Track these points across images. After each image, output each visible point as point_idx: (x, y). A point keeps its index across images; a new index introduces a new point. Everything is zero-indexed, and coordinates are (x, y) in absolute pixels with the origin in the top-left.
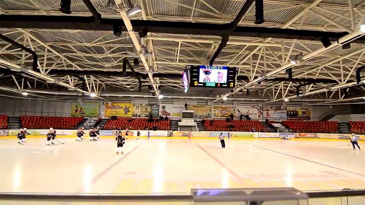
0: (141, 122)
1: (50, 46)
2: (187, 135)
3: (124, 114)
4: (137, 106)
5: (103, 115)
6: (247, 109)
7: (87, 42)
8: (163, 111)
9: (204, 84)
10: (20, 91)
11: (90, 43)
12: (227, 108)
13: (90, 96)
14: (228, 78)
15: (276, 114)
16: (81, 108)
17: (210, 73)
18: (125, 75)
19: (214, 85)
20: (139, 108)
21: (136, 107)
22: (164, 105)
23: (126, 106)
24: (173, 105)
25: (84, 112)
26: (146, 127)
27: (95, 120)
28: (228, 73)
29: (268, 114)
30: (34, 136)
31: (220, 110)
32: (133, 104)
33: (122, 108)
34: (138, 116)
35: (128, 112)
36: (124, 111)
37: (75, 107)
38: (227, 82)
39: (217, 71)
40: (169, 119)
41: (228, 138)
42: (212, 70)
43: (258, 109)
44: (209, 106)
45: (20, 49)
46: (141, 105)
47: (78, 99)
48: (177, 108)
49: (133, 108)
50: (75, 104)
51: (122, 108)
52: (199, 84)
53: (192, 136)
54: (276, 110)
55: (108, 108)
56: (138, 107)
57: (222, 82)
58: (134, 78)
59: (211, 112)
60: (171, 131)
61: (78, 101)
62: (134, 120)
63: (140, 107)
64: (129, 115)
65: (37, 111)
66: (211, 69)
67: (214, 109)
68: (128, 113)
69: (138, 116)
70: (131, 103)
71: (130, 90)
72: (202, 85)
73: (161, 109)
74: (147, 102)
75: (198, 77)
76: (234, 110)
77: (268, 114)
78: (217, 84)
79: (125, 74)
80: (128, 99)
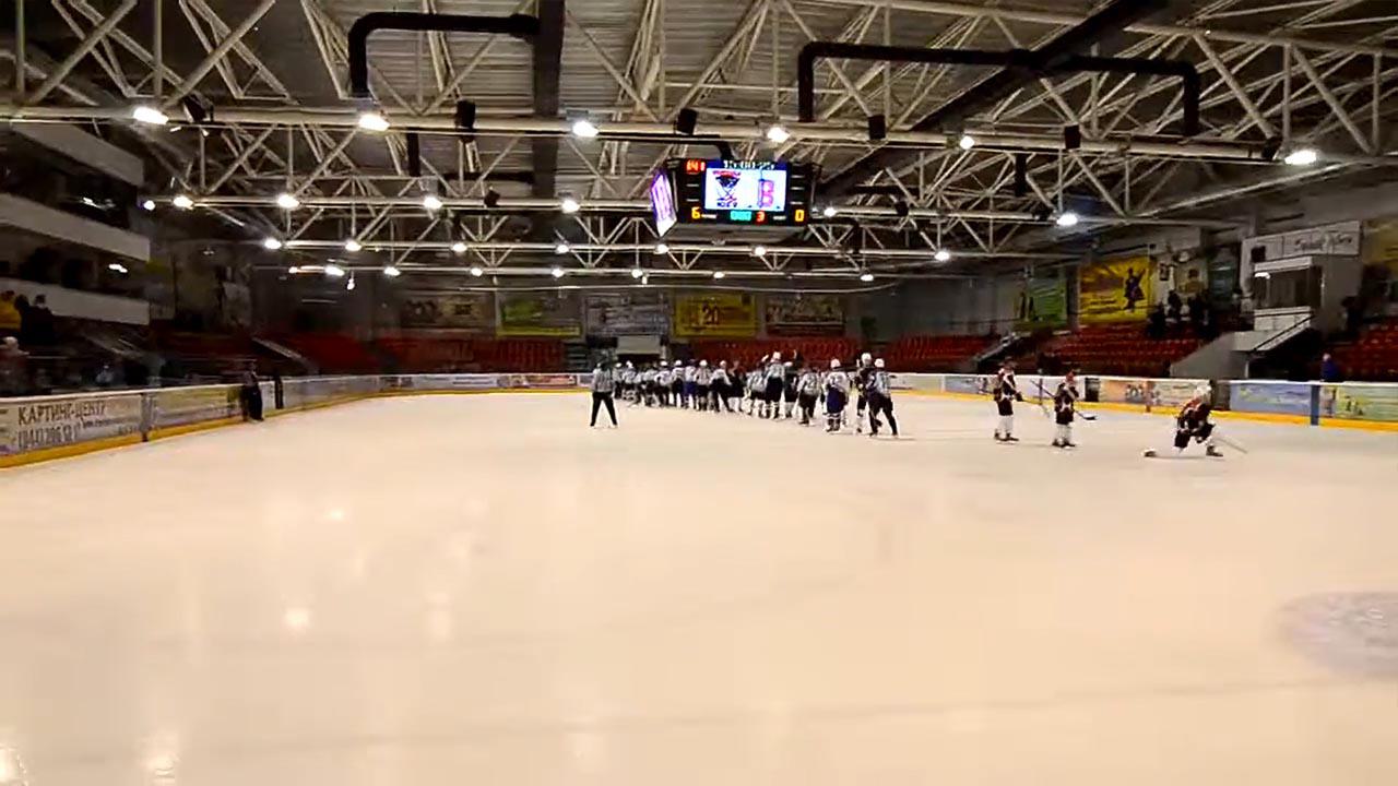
14: (789, 194)
15: (631, 318)
17: (737, 180)
19: (747, 217)
21: (1162, 271)
23: (1131, 271)
28: (790, 182)
38: (785, 208)
39: (756, 174)
41: (1308, 419)
42: (744, 172)
45: (1151, 57)
52: (704, 216)
53: (1158, 401)
54: (633, 303)
57: (772, 208)
66: (738, 171)
72: (713, 216)
75: (700, 193)
78: (755, 214)
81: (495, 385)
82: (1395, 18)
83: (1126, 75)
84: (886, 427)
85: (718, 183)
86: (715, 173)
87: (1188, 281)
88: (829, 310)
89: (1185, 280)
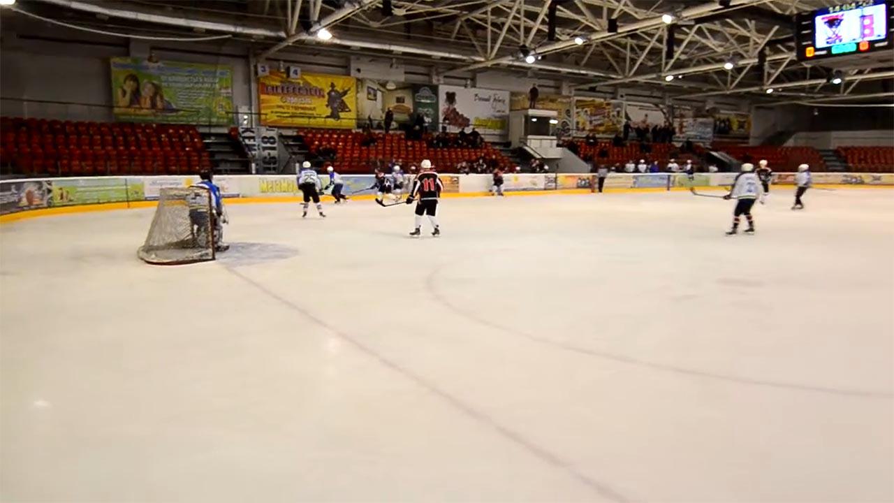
2: (587, 185)
3: (328, 117)
4: (369, 87)
6: (645, 112)
9: (829, 49)
12: (604, 106)
17: (841, 20)
20: (375, 95)
21: (369, 93)
22: (451, 89)
23: (333, 85)
27: (265, 137)
30: (101, 201)
31: (589, 113)
32: (358, 80)
33: (318, 93)
35: (342, 111)
36: (327, 106)
37: (125, 82)
42: (846, 13)
43: (664, 113)
44: (564, 101)
48: (487, 100)
49: (359, 95)
51: (318, 93)
52: (818, 53)
56: (372, 92)
59: (569, 116)
63: (379, 94)
64: (347, 120)
66: (841, 13)
67: (577, 108)
68: (342, 115)
74: (397, 76)
76: (618, 112)
85: (826, 27)
86: (823, 19)
87: (396, 104)
89: (392, 104)
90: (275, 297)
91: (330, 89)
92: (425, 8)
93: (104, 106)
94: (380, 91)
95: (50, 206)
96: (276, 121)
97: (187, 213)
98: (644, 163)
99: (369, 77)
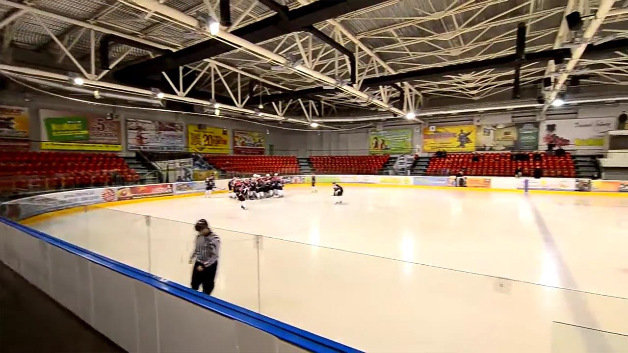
0: (499, 160)
1: (243, 70)
5: (419, 150)
7: (437, 12)
8: (548, 135)
10: (308, 121)
11: (443, 12)
13: (407, 119)
16: (383, 141)
18: (523, 60)
20: (489, 133)
21: (485, 132)
22: (551, 122)
23: (462, 131)
24: (576, 121)
25: (388, 147)
26: (516, 173)
29: (140, 138)
32: (478, 126)
33: (454, 135)
34: (487, 148)
35: (467, 143)
40: (569, 153)
46: (495, 127)
47: (378, 126)
50: (373, 135)
51: (454, 135)
55: (427, 137)
58: (368, 88)
60: (586, 180)
61: (378, 130)
62: (483, 157)
63: (492, 131)
64: (470, 148)
65: (349, 149)
69: (487, 148)
70: (472, 124)
71: (474, 100)
73: (543, 132)
74: (508, 119)
77: (141, 138)
79: (523, 58)
80: (469, 118)
81: (101, 199)
82: (626, 98)
83: (366, 88)
84: (575, 125)
88: (260, 141)
90: (76, 249)
91: (460, 132)
92: (496, 75)
93: (41, 141)
94: (492, 130)
95: (304, 183)
96: (430, 150)
97: (207, 191)
98: (445, 159)
99: (484, 123)
